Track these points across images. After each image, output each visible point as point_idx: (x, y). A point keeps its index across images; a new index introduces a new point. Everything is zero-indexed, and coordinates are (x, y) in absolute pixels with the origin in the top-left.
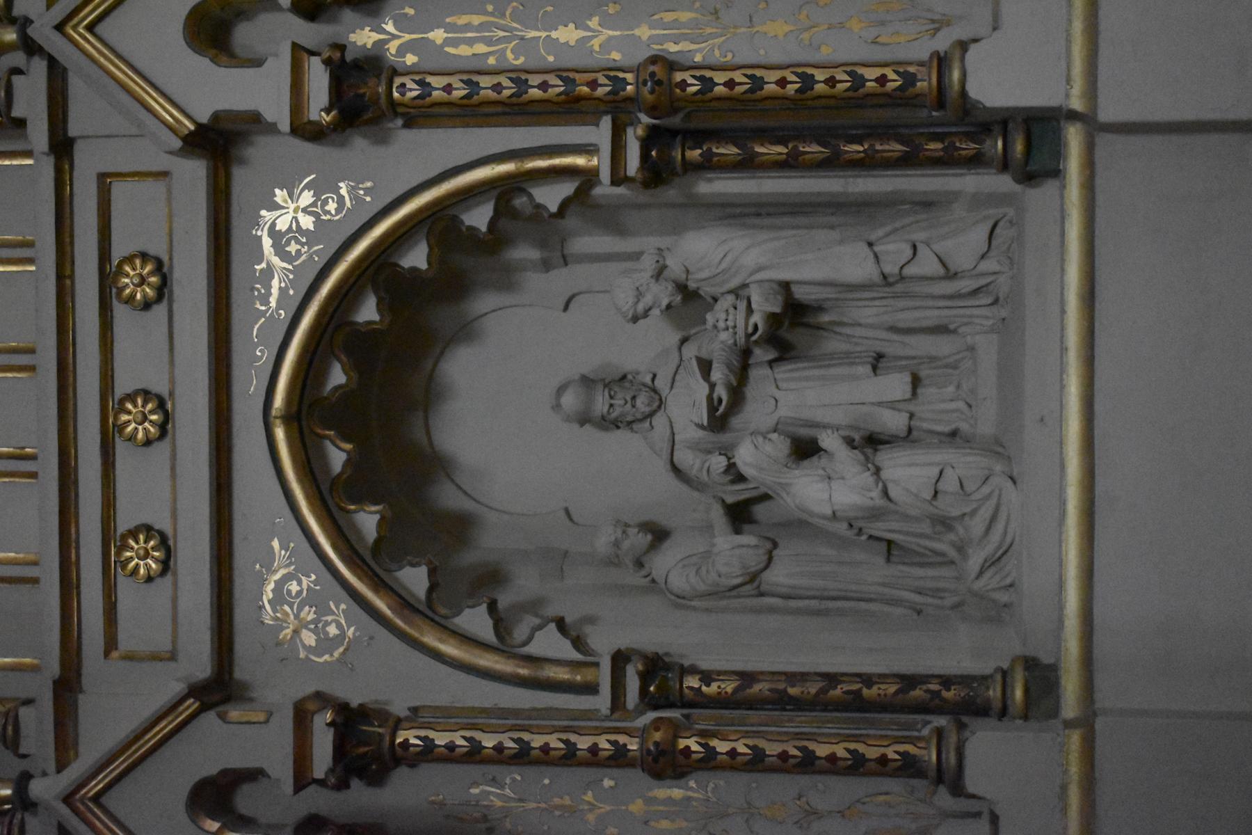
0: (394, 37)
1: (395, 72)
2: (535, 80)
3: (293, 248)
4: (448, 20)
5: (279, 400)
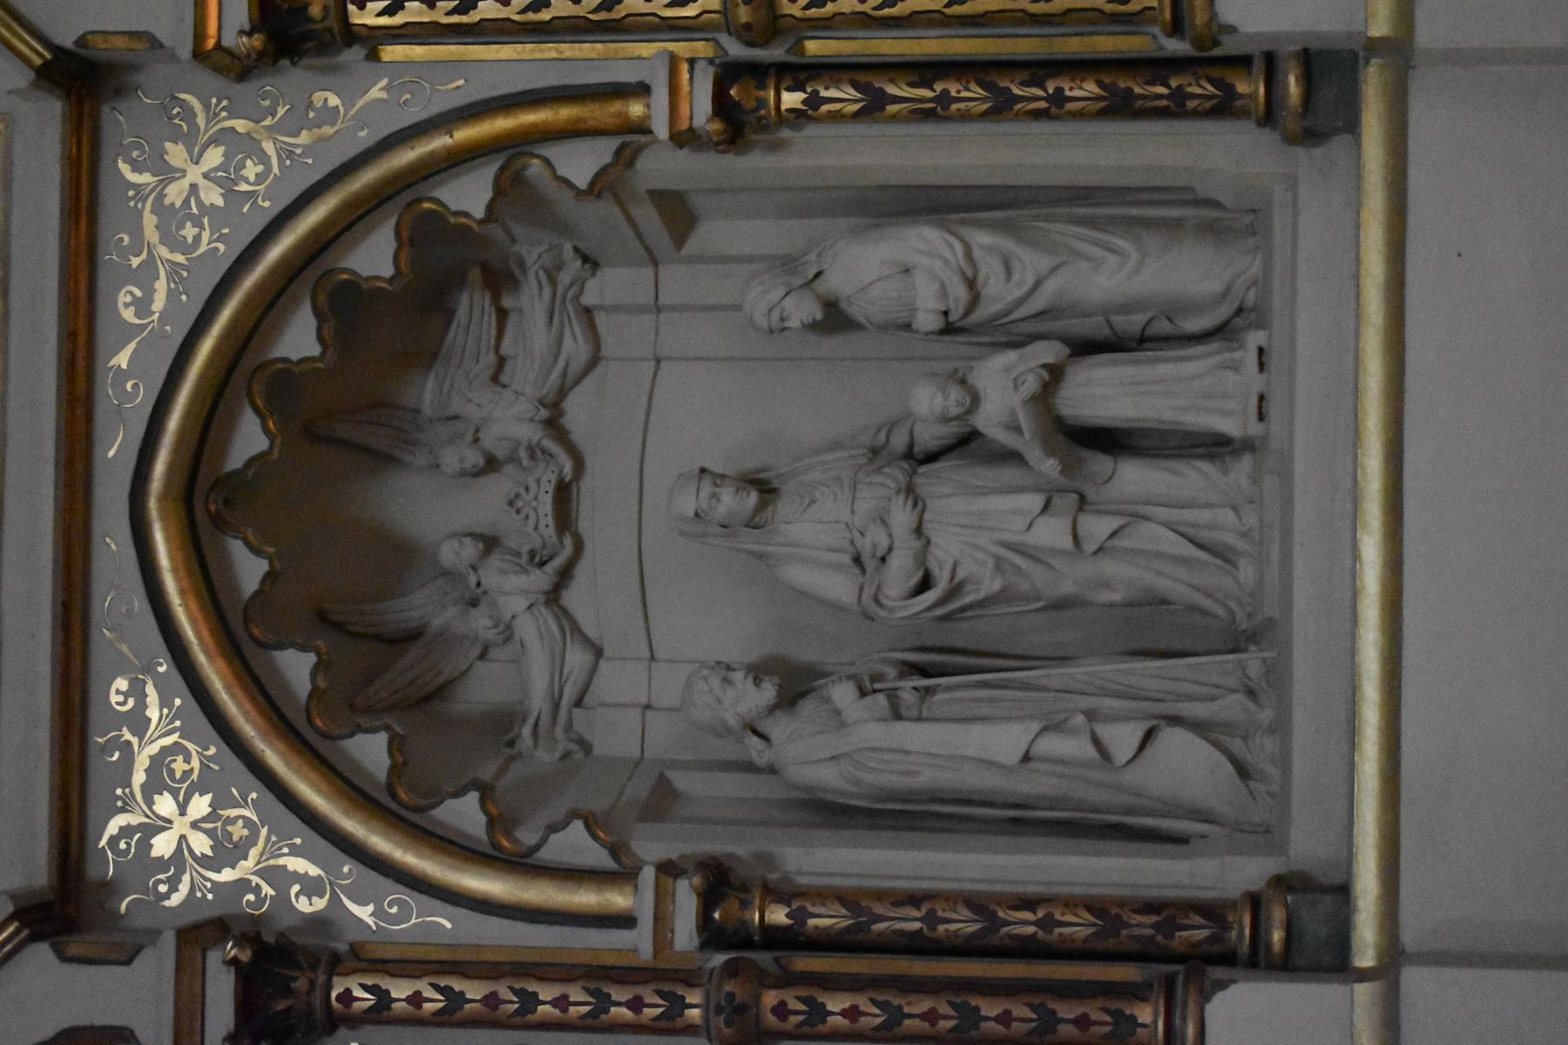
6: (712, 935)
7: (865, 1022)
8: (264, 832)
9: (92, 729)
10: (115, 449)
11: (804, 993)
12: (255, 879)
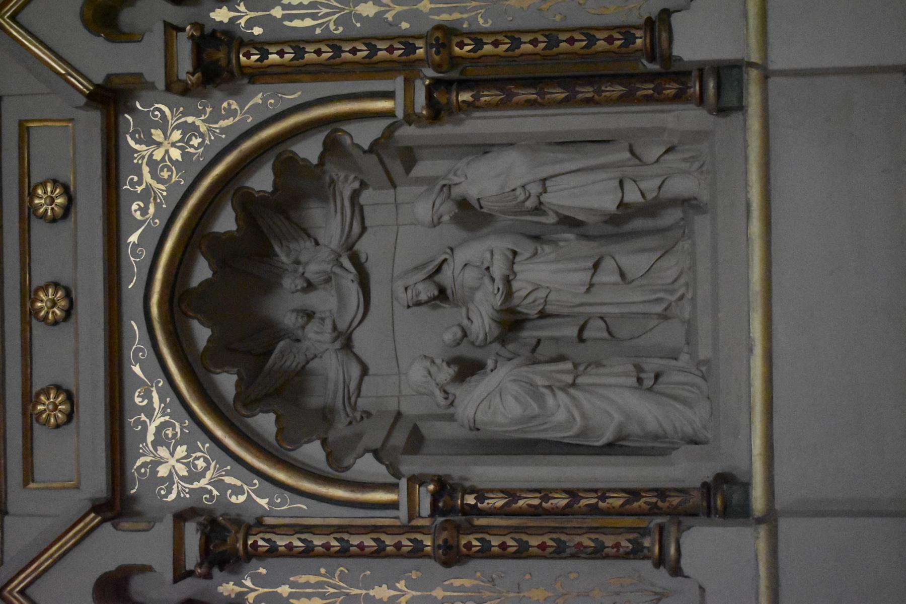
0: (253, 590)
1: (242, 43)
2: (347, 47)
3: (165, 174)
4: (292, 579)
5: (155, 311)
6: (435, 510)
7: (404, 549)
8: (213, 464)
9: (127, 414)
10: (132, 284)
11: (480, 536)
12: (210, 487)
